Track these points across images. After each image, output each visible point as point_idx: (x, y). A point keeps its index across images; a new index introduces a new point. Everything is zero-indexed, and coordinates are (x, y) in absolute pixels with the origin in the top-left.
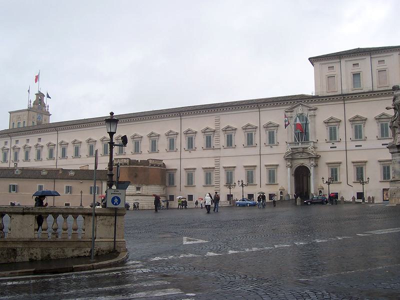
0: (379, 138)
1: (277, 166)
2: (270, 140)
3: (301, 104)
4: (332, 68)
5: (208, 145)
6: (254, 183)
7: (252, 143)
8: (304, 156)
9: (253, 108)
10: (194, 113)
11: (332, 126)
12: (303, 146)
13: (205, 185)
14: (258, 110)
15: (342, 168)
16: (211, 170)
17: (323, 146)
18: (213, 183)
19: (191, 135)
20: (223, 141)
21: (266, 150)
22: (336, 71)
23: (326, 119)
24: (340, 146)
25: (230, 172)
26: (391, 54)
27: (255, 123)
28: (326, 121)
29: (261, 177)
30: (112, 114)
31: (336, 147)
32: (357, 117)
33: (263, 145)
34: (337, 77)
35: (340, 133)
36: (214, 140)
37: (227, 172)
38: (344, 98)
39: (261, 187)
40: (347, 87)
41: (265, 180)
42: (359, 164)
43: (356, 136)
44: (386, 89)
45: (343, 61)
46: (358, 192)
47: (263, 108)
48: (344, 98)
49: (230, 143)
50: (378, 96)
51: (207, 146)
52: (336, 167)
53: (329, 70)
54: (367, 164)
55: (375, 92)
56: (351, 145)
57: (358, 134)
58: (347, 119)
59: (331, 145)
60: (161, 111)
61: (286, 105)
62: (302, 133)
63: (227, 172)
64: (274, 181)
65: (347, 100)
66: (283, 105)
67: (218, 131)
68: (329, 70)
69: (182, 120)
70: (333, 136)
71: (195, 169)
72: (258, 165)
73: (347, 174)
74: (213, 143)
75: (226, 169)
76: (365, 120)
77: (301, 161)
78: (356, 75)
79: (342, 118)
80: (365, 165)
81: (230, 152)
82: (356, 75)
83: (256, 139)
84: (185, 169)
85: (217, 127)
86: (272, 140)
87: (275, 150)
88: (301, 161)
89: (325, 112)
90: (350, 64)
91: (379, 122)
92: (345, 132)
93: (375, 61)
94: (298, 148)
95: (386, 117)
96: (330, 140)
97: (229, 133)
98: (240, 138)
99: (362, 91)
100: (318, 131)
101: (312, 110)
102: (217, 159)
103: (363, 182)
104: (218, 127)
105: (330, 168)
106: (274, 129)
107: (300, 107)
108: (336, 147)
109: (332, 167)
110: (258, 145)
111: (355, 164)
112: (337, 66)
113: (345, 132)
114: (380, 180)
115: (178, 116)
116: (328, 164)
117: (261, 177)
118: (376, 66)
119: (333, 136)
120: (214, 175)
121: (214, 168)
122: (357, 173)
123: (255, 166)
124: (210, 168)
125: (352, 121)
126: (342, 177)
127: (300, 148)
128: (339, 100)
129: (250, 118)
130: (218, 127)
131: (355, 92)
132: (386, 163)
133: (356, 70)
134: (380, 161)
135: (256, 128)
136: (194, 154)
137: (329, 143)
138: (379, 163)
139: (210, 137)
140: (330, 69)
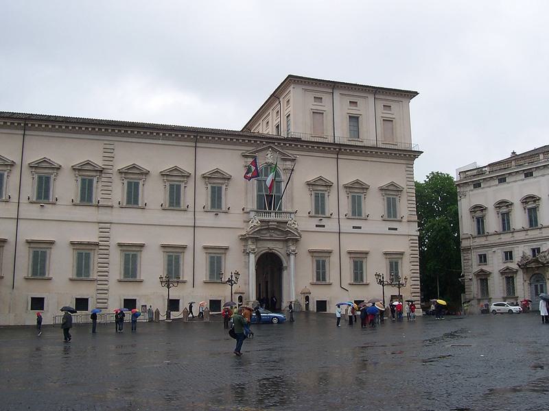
0: (206, 209)
1: (227, 249)
2: (213, 200)
3: (270, 147)
4: (320, 100)
5: (86, 196)
6: (138, 279)
7: (178, 204)
8: (276, 235)
9: (185, 140)
10: (12, 123)
11: (319, 188)
12: (279, 219)
13: (75, 277)
14: (194, 144)
15: (187, 259)
16: (93, 247)
17: (303, 222)
18: (94, 275)
19: (46, 171)
20: (118, 192)
21: (206, 219)
22: (326, 106)
23: (312, 177)
24: (331, 225)
25: (131, 254)
26: (401, 99)
27: (330, 176)
28: (207, 175)
29: (195, 267)
30: (514, 153)
31: (324, 226)
32: (134, 167)
33: (24, 200)
34: (326, 115)
35: (331, 204)
36: (100, 187)
37: (211, 257)
38: (338, 150)
39: (375, 294)
40: (342, 134)
41: (203, 273)
42: (358, 255)
43: (353, 212)
44: (393, 147)
45: (337, 94)
46: (126, 298)
47: (204, 141)
48: (338, 150)
49: (133, 198)
50: (381, 156)
51: (82, 199)
52: (324, 259)
53: (315, 101)
54: (369, 257)
55: (337, 144)
56: (347, 226)
57: (357, 211)
58: (199, 173)
59: (316, 221)
60: (16, 115)
61: (246, 145)
62: (269, 200)
63: (169, 256)
64: (134, 274)
65: (30, 129)
66: (241, 144)
67: (110, 171)
68: (315, 101)
69: (26, 137)
70: (320, 207)
71: (52, 243)
72: (190, 245)
73: (338, 270)
74: (98, 195)
75: (125, 248)
76: (12, 165)
77: (270, 245)
78: (354, 119)
79: (17, 160)
80: (225, 254)
81: (132, 215)
82: (354, 119)
83: (187, 197)
84: (28, 242)
85: (107, 163)
86: (391, 212)
87: (223, 220)
88: (270, 245)
89: (309, 169)
90: (310, 96)
91: (386, 194)
92: (337, 203)
93: (380, 105)
94: (269, 222)
95: (48, 165)
96: (316, 213)
97: (134, 179)
98: (153, 192)
99: (396, 147)
100: (298, 201)
101: (289, 160)
102: (104, 226)
103: (399, 284)
104: (111, 163)
105: (31, 250)
106: (222, 184)
107: (269, 152)
108: (324, 226)
109: (318, 259)
110: (191, 209)
111: (352, 256)
112: (326, 99)
113: (337, 203)
114: (349, 282)
115: (191, 141)
116: (311, 252)
117: (195, 267)
118: (311, 104)
119: (320, 207)
120: (95, 259)
121: (97, 245)
122: (362, 273)
123: (184, 247)
124: (89, 244)
125: (34, 167)
126: (332, 275)
127: (273, 221)
128: (16, 128)
129: (178, 157)
130: (111, 163)
131: (353, 143)
132: (394, 256)
133: (354, 112)
134: (386, 254)
135: (12, 164)
136: (50, 212)
137: (313, 219)
138: (163, 250)
139: (91, 182)
140: (317, 100)
